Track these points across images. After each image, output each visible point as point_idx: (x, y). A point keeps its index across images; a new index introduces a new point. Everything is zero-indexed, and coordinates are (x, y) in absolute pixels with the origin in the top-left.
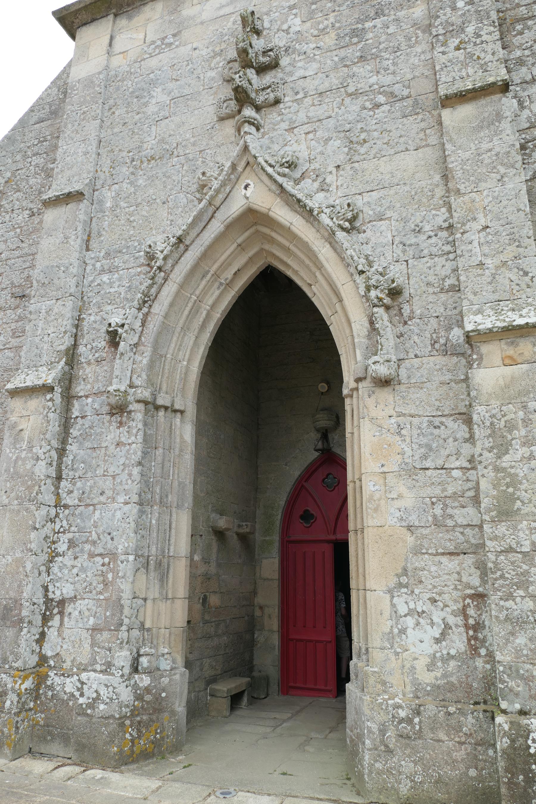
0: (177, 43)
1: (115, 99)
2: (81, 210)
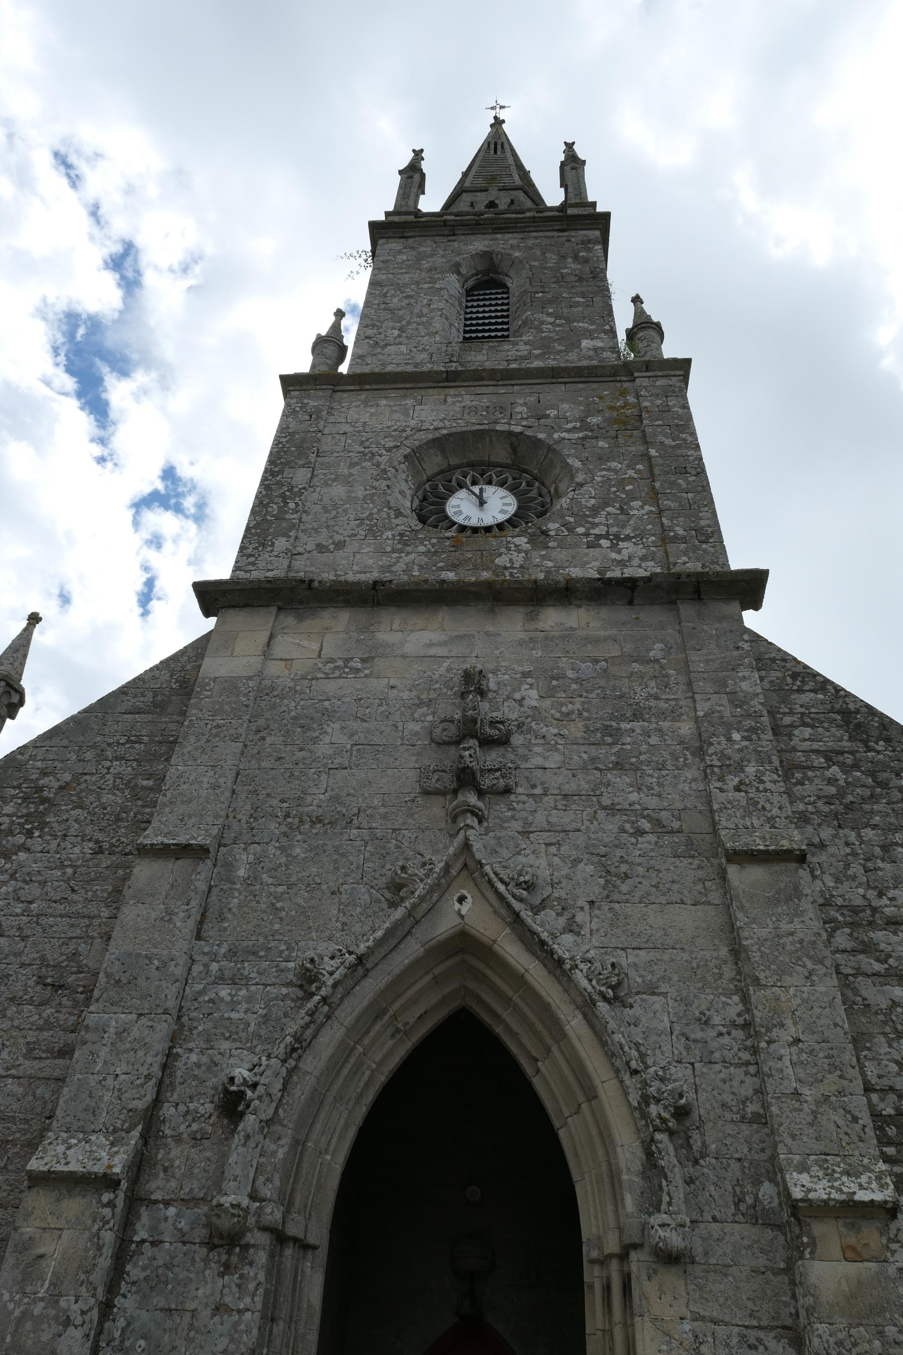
0: (367, 672)
1: (267, 719)
2: (202, 875)
